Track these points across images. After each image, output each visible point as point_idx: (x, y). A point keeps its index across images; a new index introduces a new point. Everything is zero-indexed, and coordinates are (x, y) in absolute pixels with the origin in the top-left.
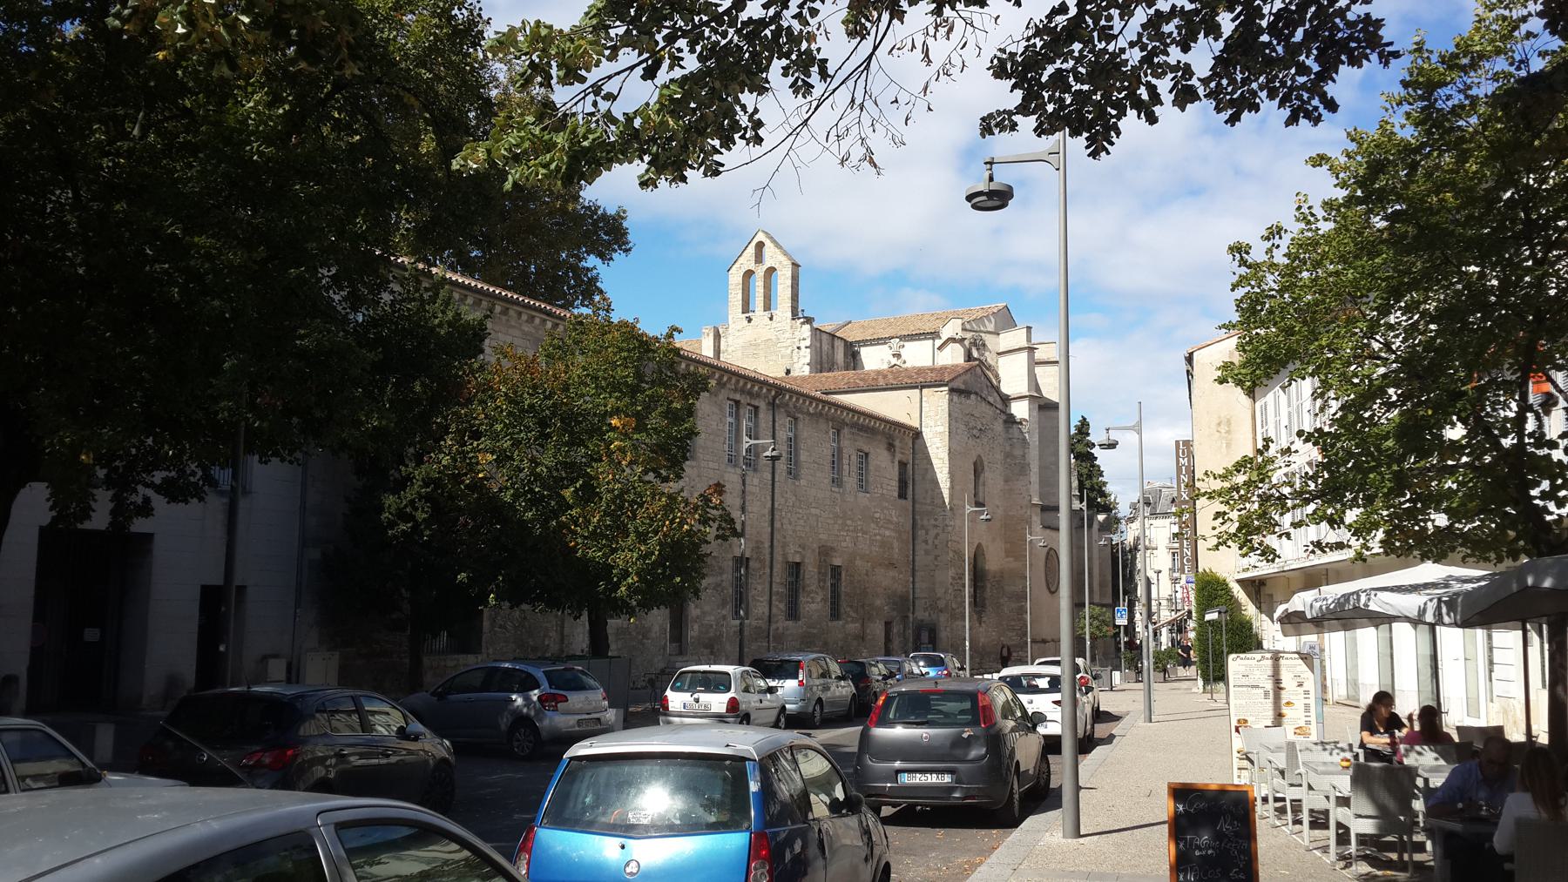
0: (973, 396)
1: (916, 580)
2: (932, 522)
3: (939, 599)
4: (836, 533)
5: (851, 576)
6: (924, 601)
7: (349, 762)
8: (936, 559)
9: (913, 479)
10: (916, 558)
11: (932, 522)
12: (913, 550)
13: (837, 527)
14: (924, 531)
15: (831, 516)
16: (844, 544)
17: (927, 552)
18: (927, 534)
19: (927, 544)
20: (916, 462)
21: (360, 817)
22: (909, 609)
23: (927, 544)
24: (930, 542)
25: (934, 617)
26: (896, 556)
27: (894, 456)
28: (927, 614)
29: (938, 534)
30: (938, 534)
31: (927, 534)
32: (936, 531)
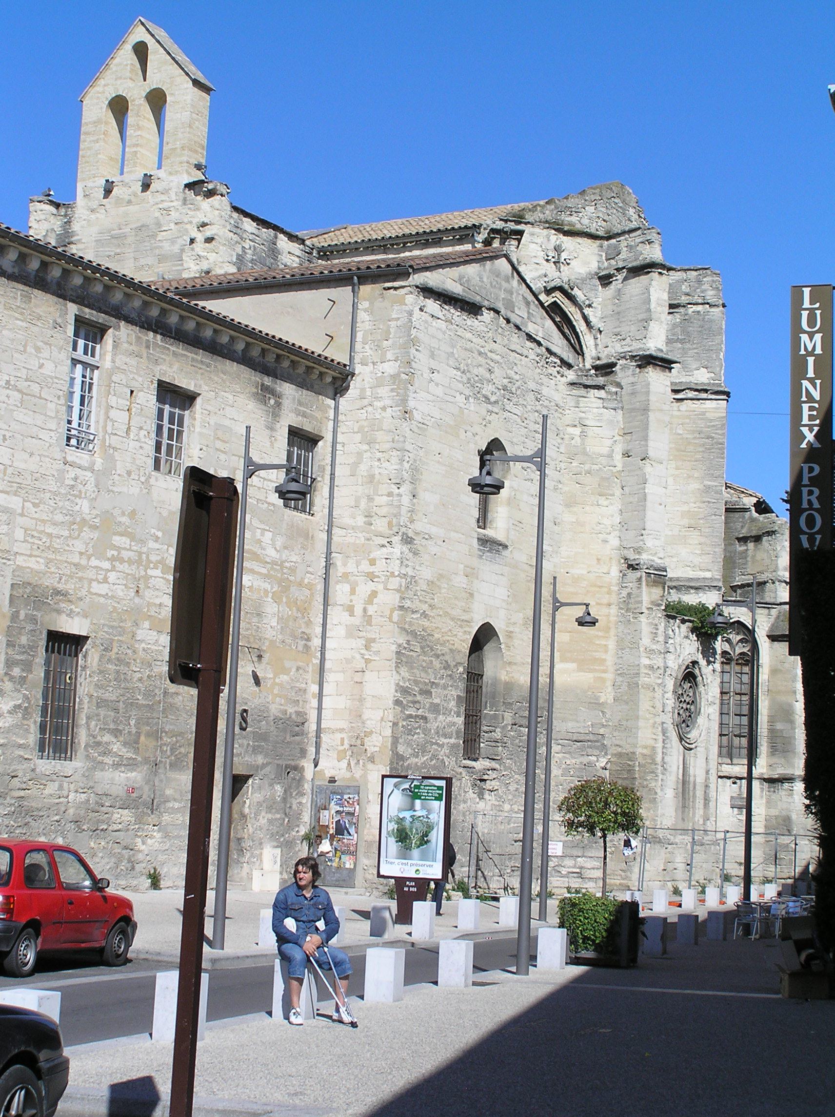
0: (487, 316)
1: (327, 689)
2: (365, 567)
3: (368, 734)
4: (76, 559)
5: (120, 661)
6: (339, 736)
7: (105, 892)
8: (367, 647)
9: (332, 474)
10: (328, 644)
11: (365, 567)
12: (324, 625)
13: (79, 546)
14: (346, 588)
15: (59, 518)
16: (103, 589)
17: (352, 632)
18: (353, 592)
19: (352, 614)
20: (340, 437)
21: (88, 970)
22: (303, 753)
23: (352, 614)
24: (358, 610)
25: (358, 773)
26: (269, 634)
27: (276, 412)
28: (344, 764)
29: (374, 594)
30: (374, 594)
31: (353, 592)
32: (371, 586)
